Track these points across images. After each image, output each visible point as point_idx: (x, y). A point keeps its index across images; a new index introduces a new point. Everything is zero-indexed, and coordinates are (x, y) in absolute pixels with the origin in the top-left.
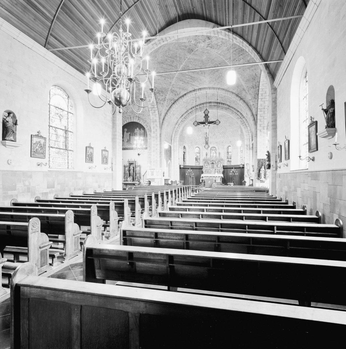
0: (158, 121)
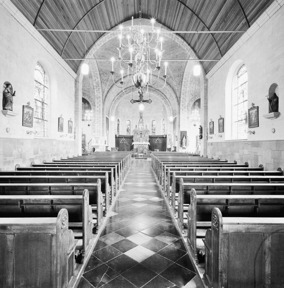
0: (101, 97)
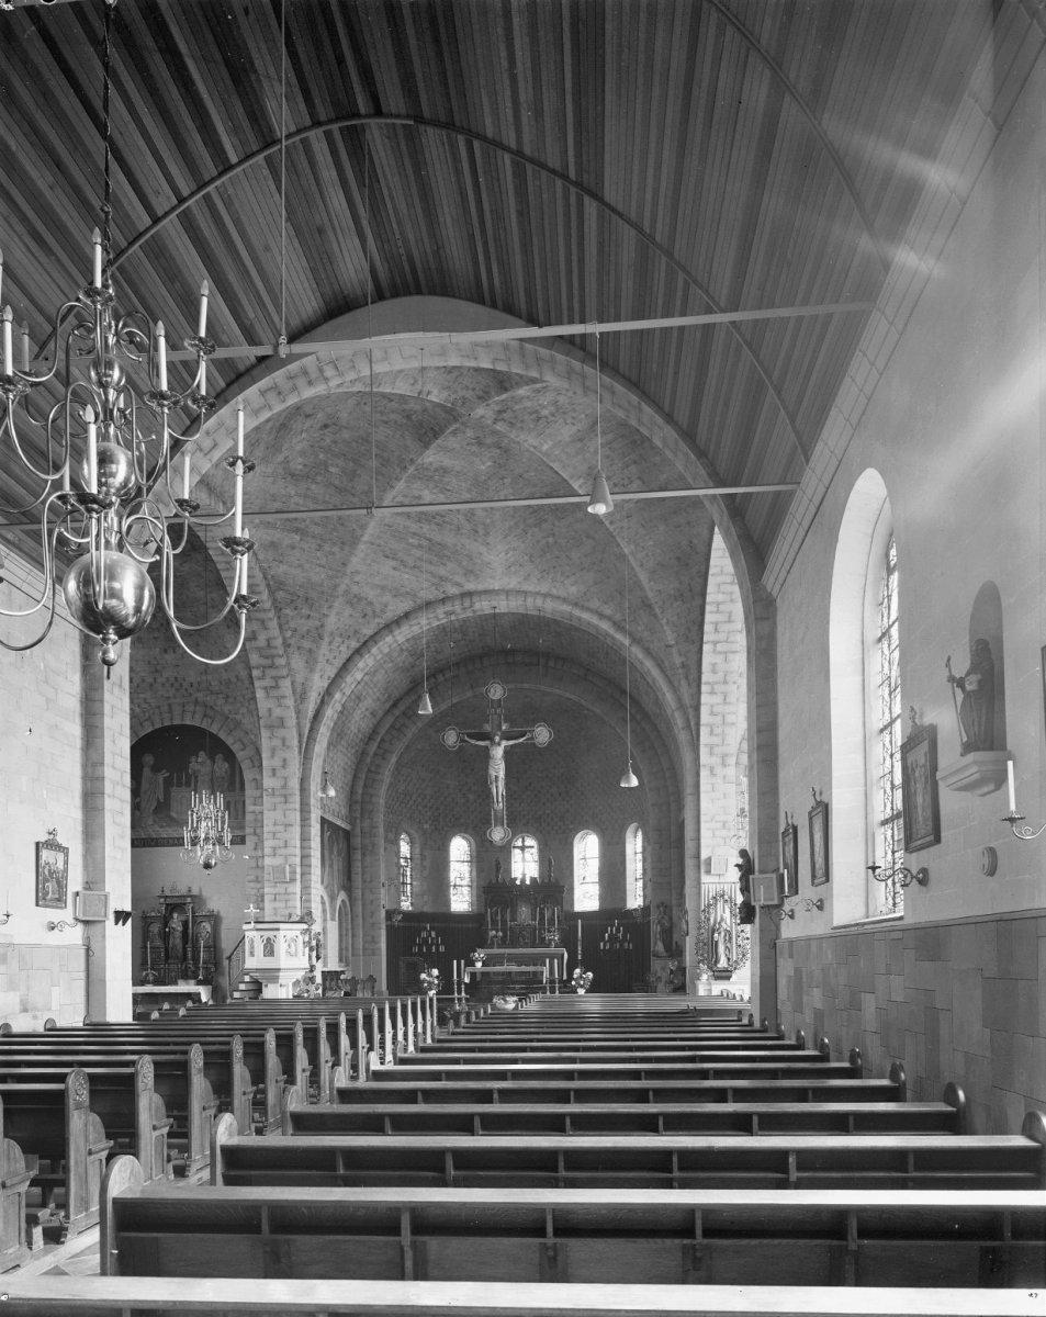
0: (292, 721)
